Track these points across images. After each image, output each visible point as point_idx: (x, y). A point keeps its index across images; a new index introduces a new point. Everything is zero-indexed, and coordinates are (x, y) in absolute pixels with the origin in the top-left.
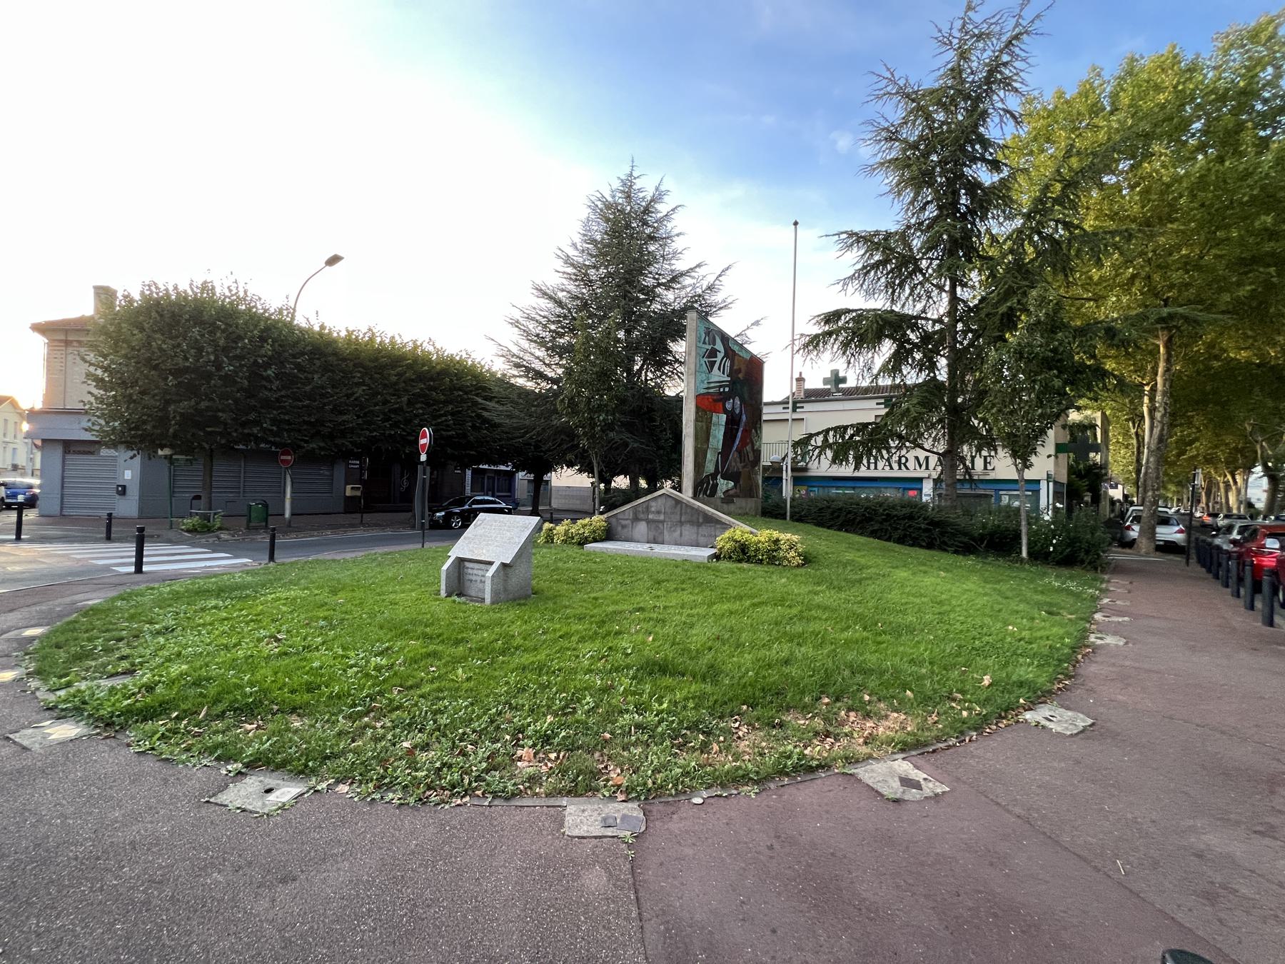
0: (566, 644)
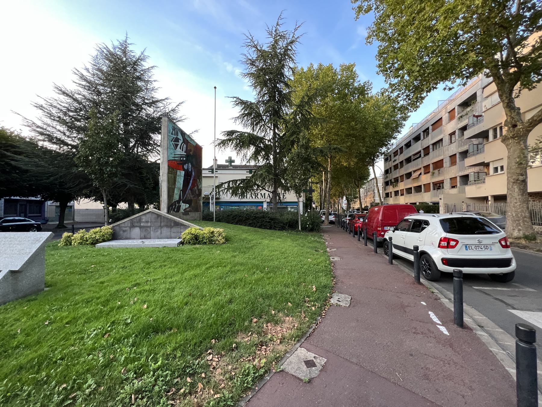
0: (70, 329)
